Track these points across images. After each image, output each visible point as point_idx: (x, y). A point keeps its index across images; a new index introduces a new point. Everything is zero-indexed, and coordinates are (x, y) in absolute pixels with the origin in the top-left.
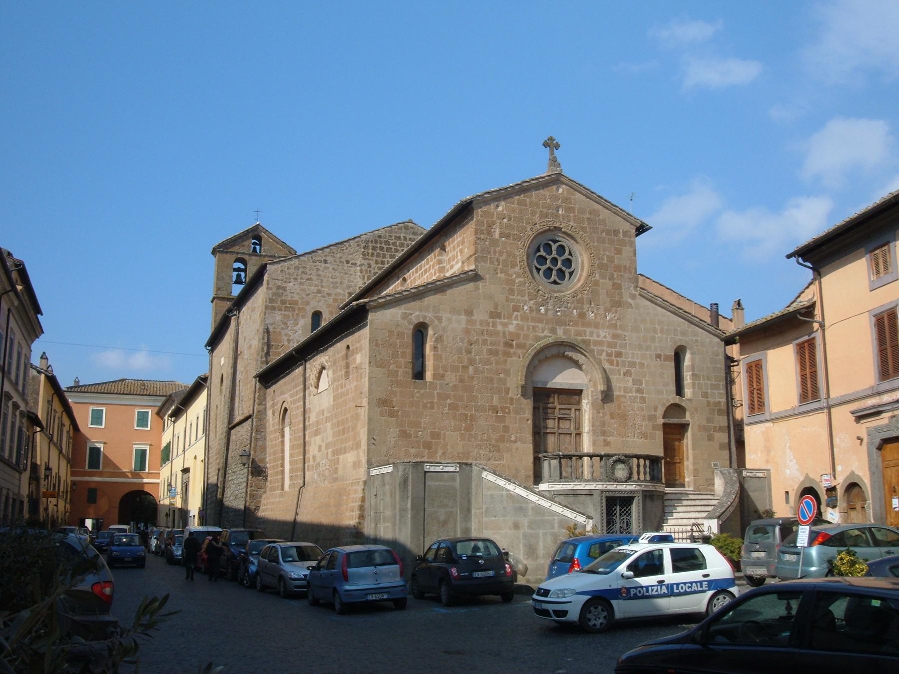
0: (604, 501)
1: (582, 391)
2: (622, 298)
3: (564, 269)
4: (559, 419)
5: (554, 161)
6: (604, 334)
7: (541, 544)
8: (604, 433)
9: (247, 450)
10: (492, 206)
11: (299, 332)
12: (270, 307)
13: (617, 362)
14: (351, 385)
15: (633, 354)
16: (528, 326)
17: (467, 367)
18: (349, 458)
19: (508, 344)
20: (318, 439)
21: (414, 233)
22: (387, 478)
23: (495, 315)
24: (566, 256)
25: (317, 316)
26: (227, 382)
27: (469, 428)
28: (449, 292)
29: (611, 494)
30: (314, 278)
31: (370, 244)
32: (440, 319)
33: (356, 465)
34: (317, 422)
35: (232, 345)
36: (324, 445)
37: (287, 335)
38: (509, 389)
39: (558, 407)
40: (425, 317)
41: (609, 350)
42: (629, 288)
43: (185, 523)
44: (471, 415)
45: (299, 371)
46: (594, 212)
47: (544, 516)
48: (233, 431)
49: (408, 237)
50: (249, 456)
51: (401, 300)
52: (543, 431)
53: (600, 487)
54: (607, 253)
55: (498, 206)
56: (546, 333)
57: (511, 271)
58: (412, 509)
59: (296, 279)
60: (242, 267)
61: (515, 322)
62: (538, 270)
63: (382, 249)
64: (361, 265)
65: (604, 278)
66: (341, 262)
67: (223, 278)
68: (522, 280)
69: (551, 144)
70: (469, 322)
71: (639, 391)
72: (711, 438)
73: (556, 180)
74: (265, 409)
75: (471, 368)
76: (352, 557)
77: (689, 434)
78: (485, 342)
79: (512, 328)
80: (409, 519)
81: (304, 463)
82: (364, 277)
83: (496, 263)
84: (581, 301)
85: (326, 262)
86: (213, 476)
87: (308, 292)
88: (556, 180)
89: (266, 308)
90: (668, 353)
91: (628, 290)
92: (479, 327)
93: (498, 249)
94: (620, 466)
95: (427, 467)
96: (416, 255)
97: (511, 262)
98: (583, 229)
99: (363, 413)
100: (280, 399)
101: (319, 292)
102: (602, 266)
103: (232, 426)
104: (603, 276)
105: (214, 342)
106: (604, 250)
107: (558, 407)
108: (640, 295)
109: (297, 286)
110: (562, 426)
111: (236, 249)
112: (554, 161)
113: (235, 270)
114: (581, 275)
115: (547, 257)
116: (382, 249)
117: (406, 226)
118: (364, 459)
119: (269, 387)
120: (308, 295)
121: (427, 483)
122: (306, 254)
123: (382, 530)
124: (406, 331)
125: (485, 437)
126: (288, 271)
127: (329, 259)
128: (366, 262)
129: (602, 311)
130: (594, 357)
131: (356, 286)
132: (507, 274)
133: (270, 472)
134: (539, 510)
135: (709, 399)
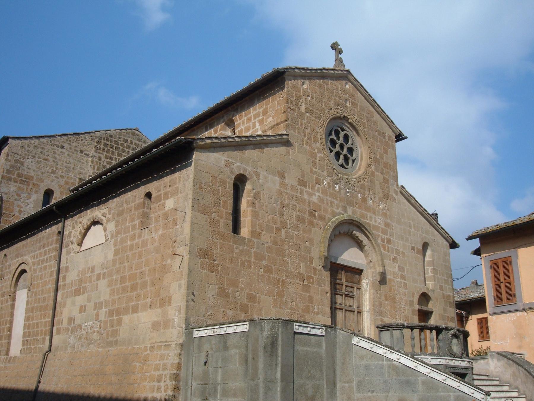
3: (349, 156)
4: (346, 295)
10: (300, 81)
13: (388, 248)
14: (154, 234)
16: (327, 200)
18: (146, 318)
19: (312, 214)
20: (80, 300)
21: (139, 140)
22: (231, 342)
25: (48, 194)
27: (281, 294)
28: (265, 150)
30: (51, 159)
31: (102, 140)
32: (258, 175)
34: (80, 281)
36: (90, 306)
37: (18, 206)
38: (313, 259)
41: (384, 236)
42: (393, 185)
45: (55, 229)
47: (438, 391)
49: (134, 141)
55: (303, 84)
56: (340, 210)
57: (314, 145)
58: (282, 380)
59: (34, 157)
61: (317, 194)
62: (331, 151)
63: (112, 147)
64: (93, 157)
66: (75, 150)
68: (322, 155)
69: (335, 47)
70: (282, 184)
71: (403, 277)
73: (345, 76)
75: (283, 232)
79: (315, 199)
80: (279, 393)
85: (62, 147)
87: (43, 171)
90: (419, 247)
93: (304, 122)
94: (455, 341)
95: (297, 328)
98: (364, 125)
100: (20, 260)
102: (376, 161)
107: (345, 284)
108: (401, 192)
114: (360, 165)
116: (112, 147)
117: (134, 132)
118: (176, 316)
120: (43, 173)
121: (297, 347)
122: (45, 136)
124: (228, 180)
126: (27, 148)
128: (97, 155)
132: (311, 147)
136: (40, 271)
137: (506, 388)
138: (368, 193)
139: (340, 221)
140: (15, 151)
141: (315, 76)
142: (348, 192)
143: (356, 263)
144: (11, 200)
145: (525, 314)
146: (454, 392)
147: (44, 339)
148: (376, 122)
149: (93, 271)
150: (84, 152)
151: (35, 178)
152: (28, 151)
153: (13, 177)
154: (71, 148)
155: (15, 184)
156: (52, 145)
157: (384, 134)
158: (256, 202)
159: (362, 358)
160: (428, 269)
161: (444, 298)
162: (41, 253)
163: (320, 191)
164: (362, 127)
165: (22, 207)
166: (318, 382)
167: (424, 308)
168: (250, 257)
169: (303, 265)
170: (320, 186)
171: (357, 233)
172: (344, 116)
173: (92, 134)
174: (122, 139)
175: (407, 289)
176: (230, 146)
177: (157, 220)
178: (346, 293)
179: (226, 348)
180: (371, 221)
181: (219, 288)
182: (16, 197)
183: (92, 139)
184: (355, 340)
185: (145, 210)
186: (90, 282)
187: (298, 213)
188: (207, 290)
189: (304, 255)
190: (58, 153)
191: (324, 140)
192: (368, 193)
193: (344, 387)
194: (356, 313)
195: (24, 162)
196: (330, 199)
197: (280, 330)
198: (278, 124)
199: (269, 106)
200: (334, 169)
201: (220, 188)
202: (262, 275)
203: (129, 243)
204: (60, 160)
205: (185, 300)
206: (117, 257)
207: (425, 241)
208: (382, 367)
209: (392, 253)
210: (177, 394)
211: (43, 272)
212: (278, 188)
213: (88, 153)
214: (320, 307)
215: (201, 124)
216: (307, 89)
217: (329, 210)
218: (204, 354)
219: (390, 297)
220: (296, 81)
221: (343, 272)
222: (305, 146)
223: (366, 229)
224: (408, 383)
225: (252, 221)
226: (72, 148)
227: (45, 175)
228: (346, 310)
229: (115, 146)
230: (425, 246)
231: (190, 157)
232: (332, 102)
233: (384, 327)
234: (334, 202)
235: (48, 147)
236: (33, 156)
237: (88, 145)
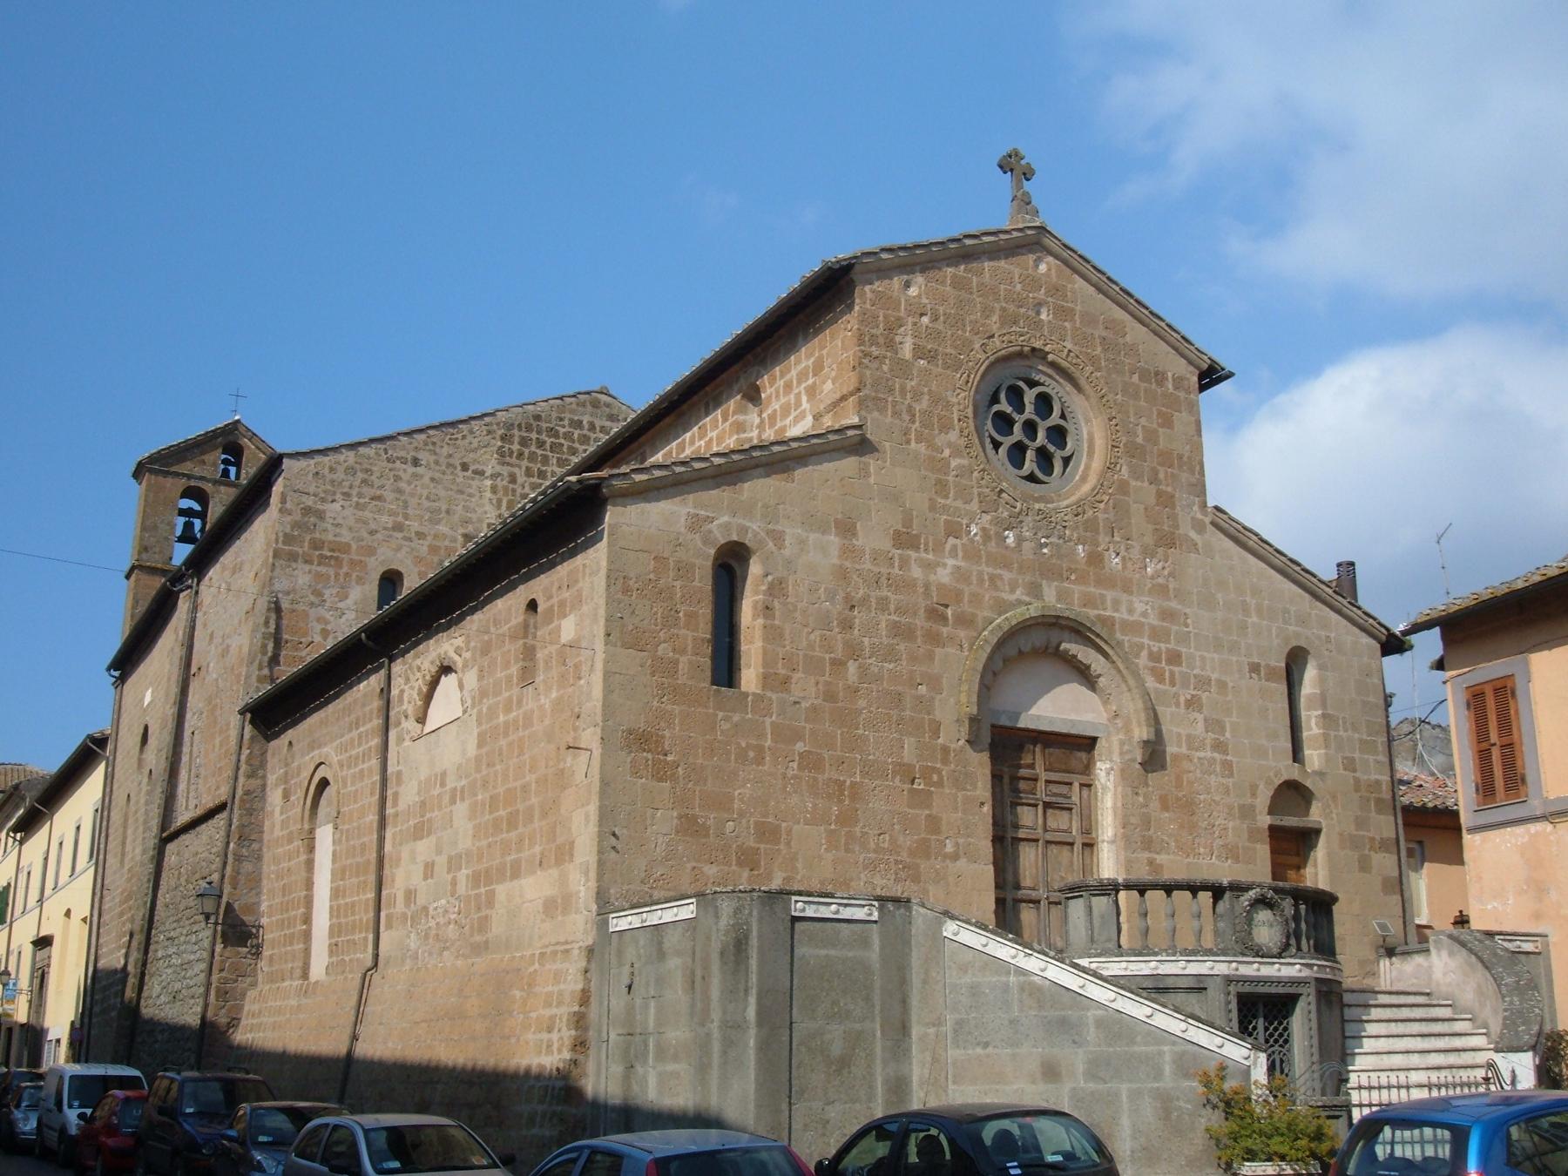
0: (1234, 1006)
1: (1094, 740)
2: (1177, 527)
3: (1051, 448)
4: (1047, 805)
6: (1141, 608)
7: (1125, 1122)
8: (1148, 844)
9: (216, 877)
10: (897, 281)
11: (349, 611)
12: (284, 554)
13: (1172, 674)
14: (543, 699)
15: (1203, 658)
16: (980, 573)
18: (534, 888)
19: (936, 615)
20: (424, 848)
22: (672, 940)
24: (1054, 419)
26: (160, 739)
29: (1247, 989)
30: (389, 495)
31: (516, 432)
32: (778, 538)
33: (555, 907)
34: (423, 803)
35: (179, 652)
36: (441, 861)
42: (1190, 506)
43: (35, 1058)
44: (853, 784)
45: (374, 682)
46: (1110, 325)
47: (1132, 1042)
48: (170, 847)
49: (598, 423)
50: (220, 897)
53: (1222, 969)
54: (1143, 421)
55: (907, 285)
56: (1019, 594)
57: (940, 440)
58: (760, 1022)
59: (347, 495)
60: (197, 507)
61: (951, 562)
62: (996, 445)
63: (541, 444)
64: (494, 476)
65: (1139, 478)
67: (155, 527)
68: (965, 462)
69: (1012, 165)
70: (848, 552)
71: (1219, 746)
72: (1364, 865)
73: (1034, 241)
74: (264, 786)
75: (852, 667)
76: (673, 1166)
78: (883, 604)
79: (943, 576)
81: (378, 910)
82: (499, 501)
85: (416, 462)
86: (111, 952)
87: (373, 526)
89: (276, 555)
90: (1273, 663)
92: (868, 566)
94: (1263, 915)
95: (798, 907)
96: (667, 420)
98: (1094, 360)
99: (585, 769)
100: (316, 756)
101: (398, 527)
102: (1134, 451)
103: (168, 835)
104: (1136, 474)
105: (126, 661)
106: (1139, 415)
107: (1043, 776)
108: (1212, 523)
109: (347, 512)
110: (1052, 824)
111: (186, 467)
113: (182, 512)
114: (1087, 467)
115: (1016, 416)
116: (541, 444)
117: (594, 399)
118: (583, 888)
119: (277, 735)
120: (372, 533)
121: (798, 951)
122: (372, 441)
123: (652, 1081)
126: (330, 477)
127: (424, 457)
128: (505, 470)
130: (1126, 660)
131: (480, 521)
132: (931, 445)
133: (269, 936)
134: (1117, 1026)
135: (1358, 774)
136: (353, 784)
137: (1459, 1027)
138: (1107, 539)
139: (1014, 622)
140: (300, 486)
142: (1046, 545)
144: (301, 607)
145: (1549, 827)
146: (1174, 1043)
147: (366, 939)
148: (1132, 349)
149: (443, 785)
150: (472, 468)
151: (354, 546)
152: (333, 481)
153: (300, 551)
154: (437, 463)
155: (307, 567)
156: (388, 460)
157: (1160, 377)
158: (776, 604)
159: (964, 968)
160: (1309, 717)
161: (1356, 791)
162: (352, 740)
163: (960, 554)
164: (1089, 369)
165: (327, 622)
166: (858, 1026)
167: (1291, 821)
168: (762, 736)
169: (909, 743)
170: (958, 541)
171: (1072, 647)
172: (1034, 350)
173: (487, 419)
174: (566, 422)
175: (1231, 775)
177: (548, 667)
178: (1047, 799)
179: (661, 955)
180: (1117, 610)
181: (680, 817)
182: (312, 598)
183: (489, 432)
184: (950, 928)
185: (530, 641)
186: (440, 808)
187: (894, 617)
190: (405, 477)
191: (971, 422)
192: (1107, 539)
193: (926, 1035)
194: (1078, 847)
195: (324, 512)
196: (990, 570)
197: (755, 913)
198: (843, 398)
199: (824, 352)
200: (1002, 491)
201: (678, 584)
202: (794, 777)
203: (502, 718)
204: (412, 495)
205: (595, 849)
206: (484, 750)
207: (1294, 643)
208: (1006, 988)
209: (1185, 685)
210: (581, 1057)
211: (359, 785)
212: (835, 561)
213: (481, 468)
214: (961, 841)
215: (695, 398)
216: (919, 296)
218: (626, 970)
219: (1178, 799)
220: (887, 281)
221: (1038, 749)
222: (913, 444)
223: (1098, 635)
224: (1063, 1024)
225: (765, 653)
226: (442, 460)
227: (379, 536)
228: (1048, 842)
229: (549, 441)
230: (1295, 661)
231: (601, 521)
232: (995, 318)
233: (1071, 889)
234: (1000, 577)
235: (380, 465)
236: (344, 494)
237: (479, 447)
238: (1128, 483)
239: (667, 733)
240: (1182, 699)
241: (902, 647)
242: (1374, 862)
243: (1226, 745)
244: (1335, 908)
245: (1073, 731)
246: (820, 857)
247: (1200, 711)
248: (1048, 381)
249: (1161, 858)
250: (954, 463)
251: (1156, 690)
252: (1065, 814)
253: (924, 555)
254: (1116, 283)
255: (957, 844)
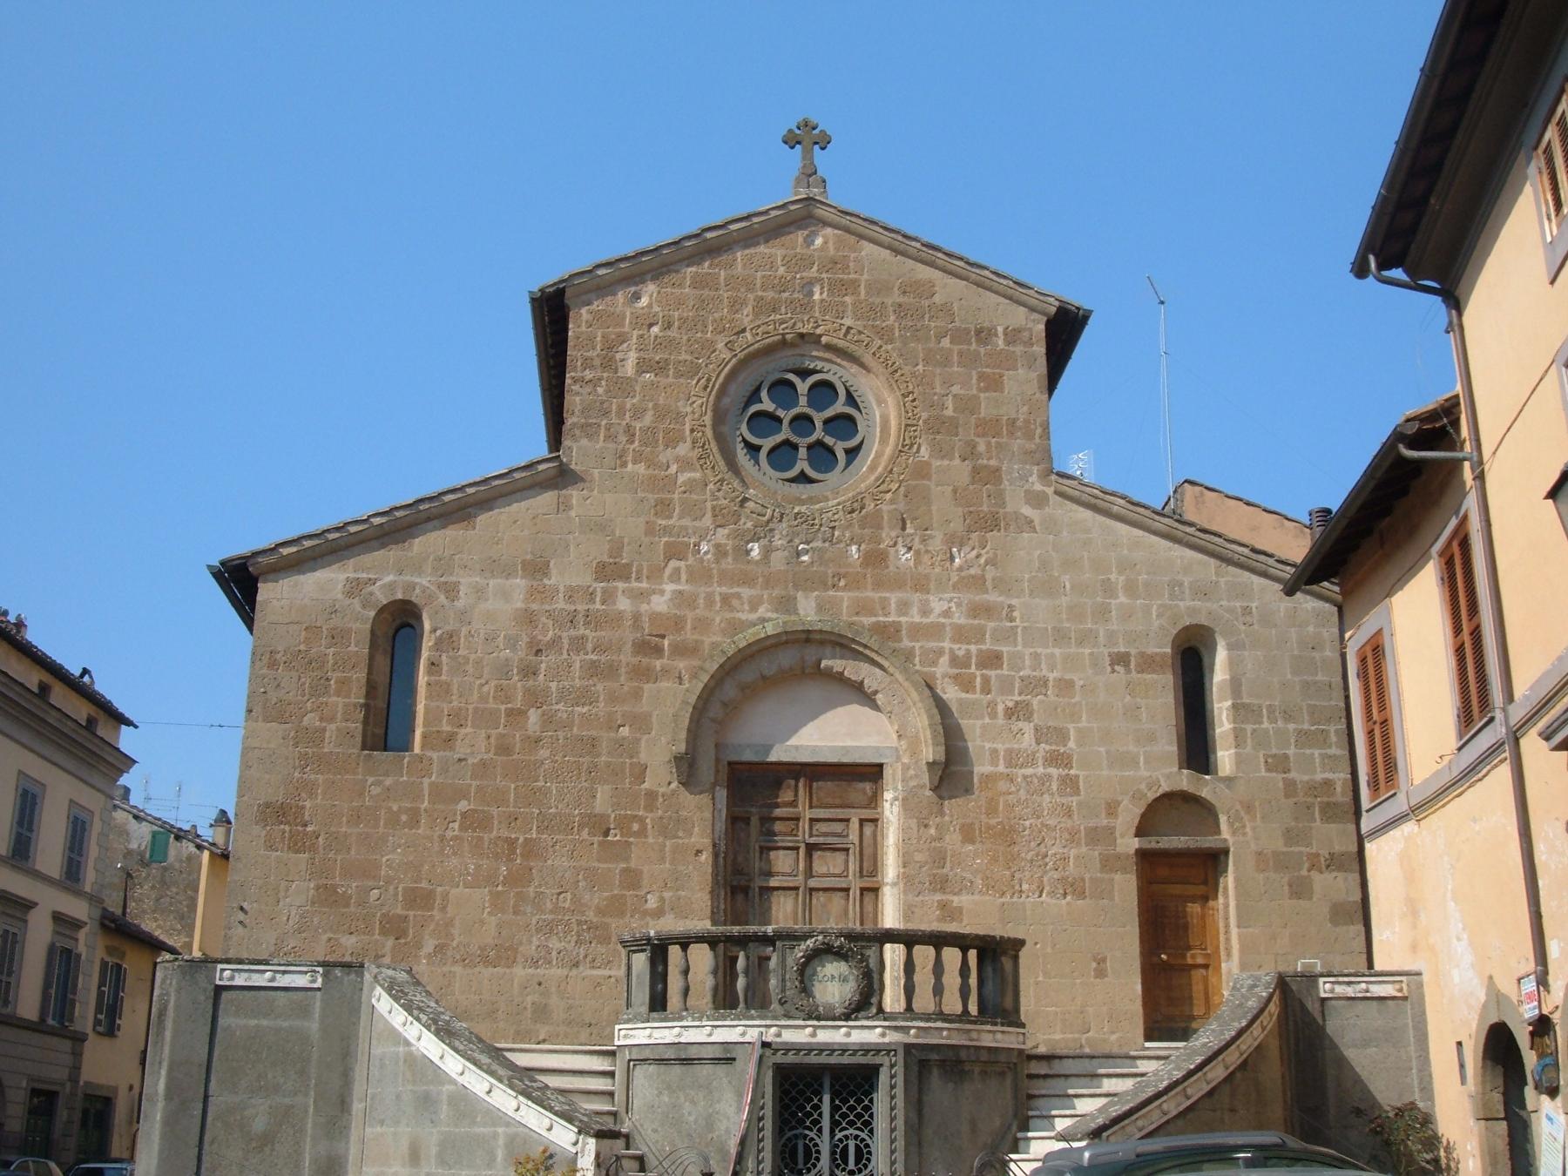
1: (880, 766)
2: (1003, 505)
4: (811, 848)
5: (809, 173)
6: (942, 605)
8: (941, 884)
15: (1036, 656)
17: (522, 713)
23: (610, 571)
27: (518, 879)
28: (483, 519)
29: (791, 1058)
32: (451, 590)
39: (808, 814)
40: (412, 586)
42: (1024, 478)
47: (473, 1123)
51: (348, 547)
52: (759, 882)
54: (956, 389)
55: (637, 297)
56: (762, 611)
57: (666, 455)
58: (169, 1096)
61: (669, 588)
62: (753, 449)
65: (948, 455)
68: (697, 475)
69: (806, 137)
71: (1055, 759)
72: (1300, 890)
75: (534, 716)
77: (1229, 880)
78: (578, 644)
80: (158, 1126)
83: (623, 438)
84: (874, 522)
88: (801, 216)
91: (1019, 488)
93: (629, 403)
97: (667, 432)
98: (885, 334)
102: (938, 426)
104: (940, 451)
112: (809, 173)
115: (781, 413)
125: (566, 901)
129: (937, 543)
132: (651, 463)
135: (1293, 775)
141: (680, 261)
143: (846, 750)
146: (508, 1125)
163: (684, 577)
166: (287, 1101)
168: (419, 797)
171: (836, 664)
172: (802, 336)
176: (361, 542)
178: (812, 840)
181: (317, 888)
188: (282, 894)
189: (608, 765)
200: (745, 500)
212: (519, 605)
214: (667, 895)
216: (650, 306)
217: (718, 620)
219: (989, 827)
222: (630, 465)
223: (865, 646)
228: (812, 890)
232: (748, 310)
234: (738, 596)
238: (928, 464)
239: (308, 804)
240: (1000, 708)
241: (600, 687)
242: (1317, 887)
243: (1070, 757)
244: (1023, 954)
245: (845, 760)
246: (482, 922)
247: (1029, 719)
248: (827, 366)
249: (962, 900)
250: (681, 479)
251: (961, 702)
252: (840, 856)
253: (635, 584)
254: (915, 239)
255: (662, 899)
